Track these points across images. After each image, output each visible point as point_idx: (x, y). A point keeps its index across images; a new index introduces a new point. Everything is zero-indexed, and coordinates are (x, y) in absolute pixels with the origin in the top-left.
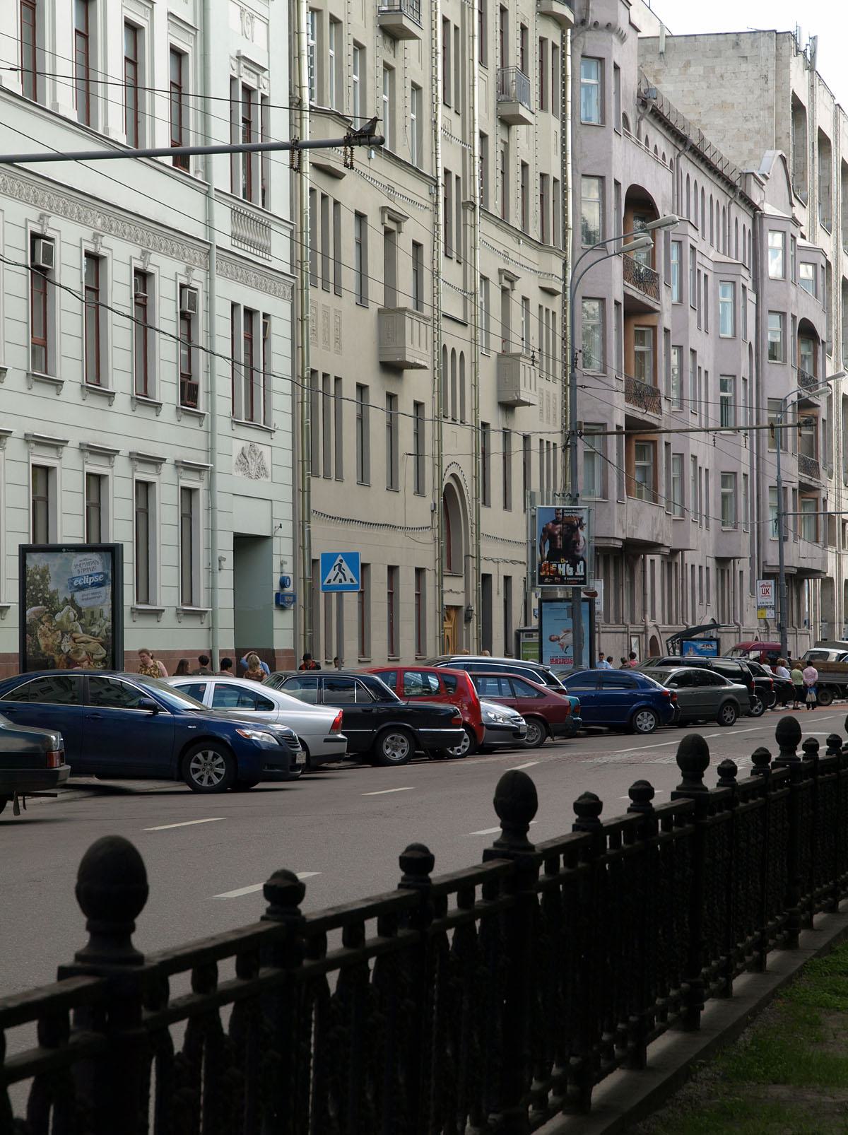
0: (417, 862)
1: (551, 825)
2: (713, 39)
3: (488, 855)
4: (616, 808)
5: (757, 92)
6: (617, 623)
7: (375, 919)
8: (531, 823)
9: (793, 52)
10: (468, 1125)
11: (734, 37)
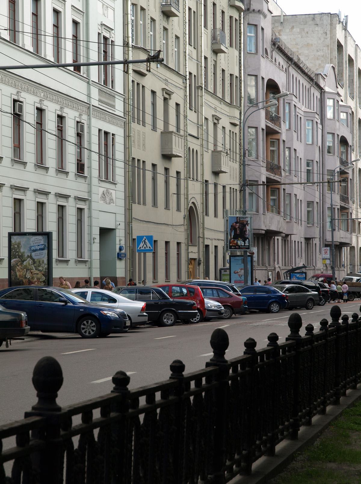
0: (177, 367)
1: (235, 352)
2: (303, 17)
3: (208, 365)
4: (262, 344)
5: (322, 39)
6: (263, 265)
7: (160, 392)
8: (226, 351)
9: (338, 22)
10: (199, 480)
11: (312, 16)
